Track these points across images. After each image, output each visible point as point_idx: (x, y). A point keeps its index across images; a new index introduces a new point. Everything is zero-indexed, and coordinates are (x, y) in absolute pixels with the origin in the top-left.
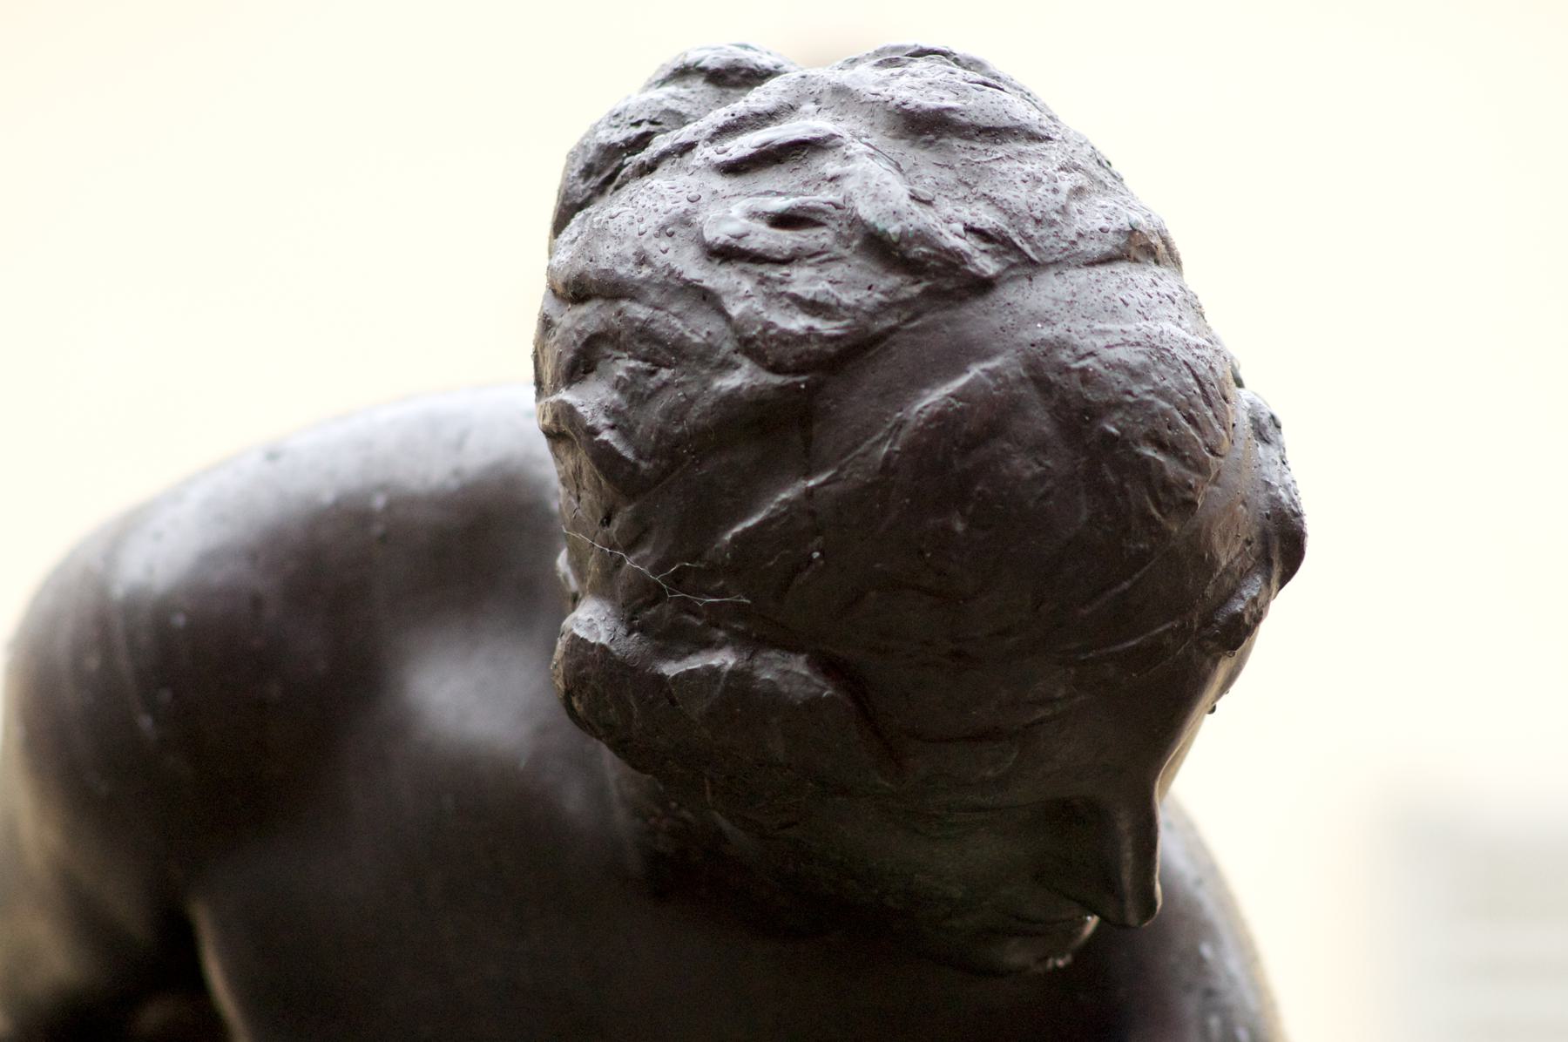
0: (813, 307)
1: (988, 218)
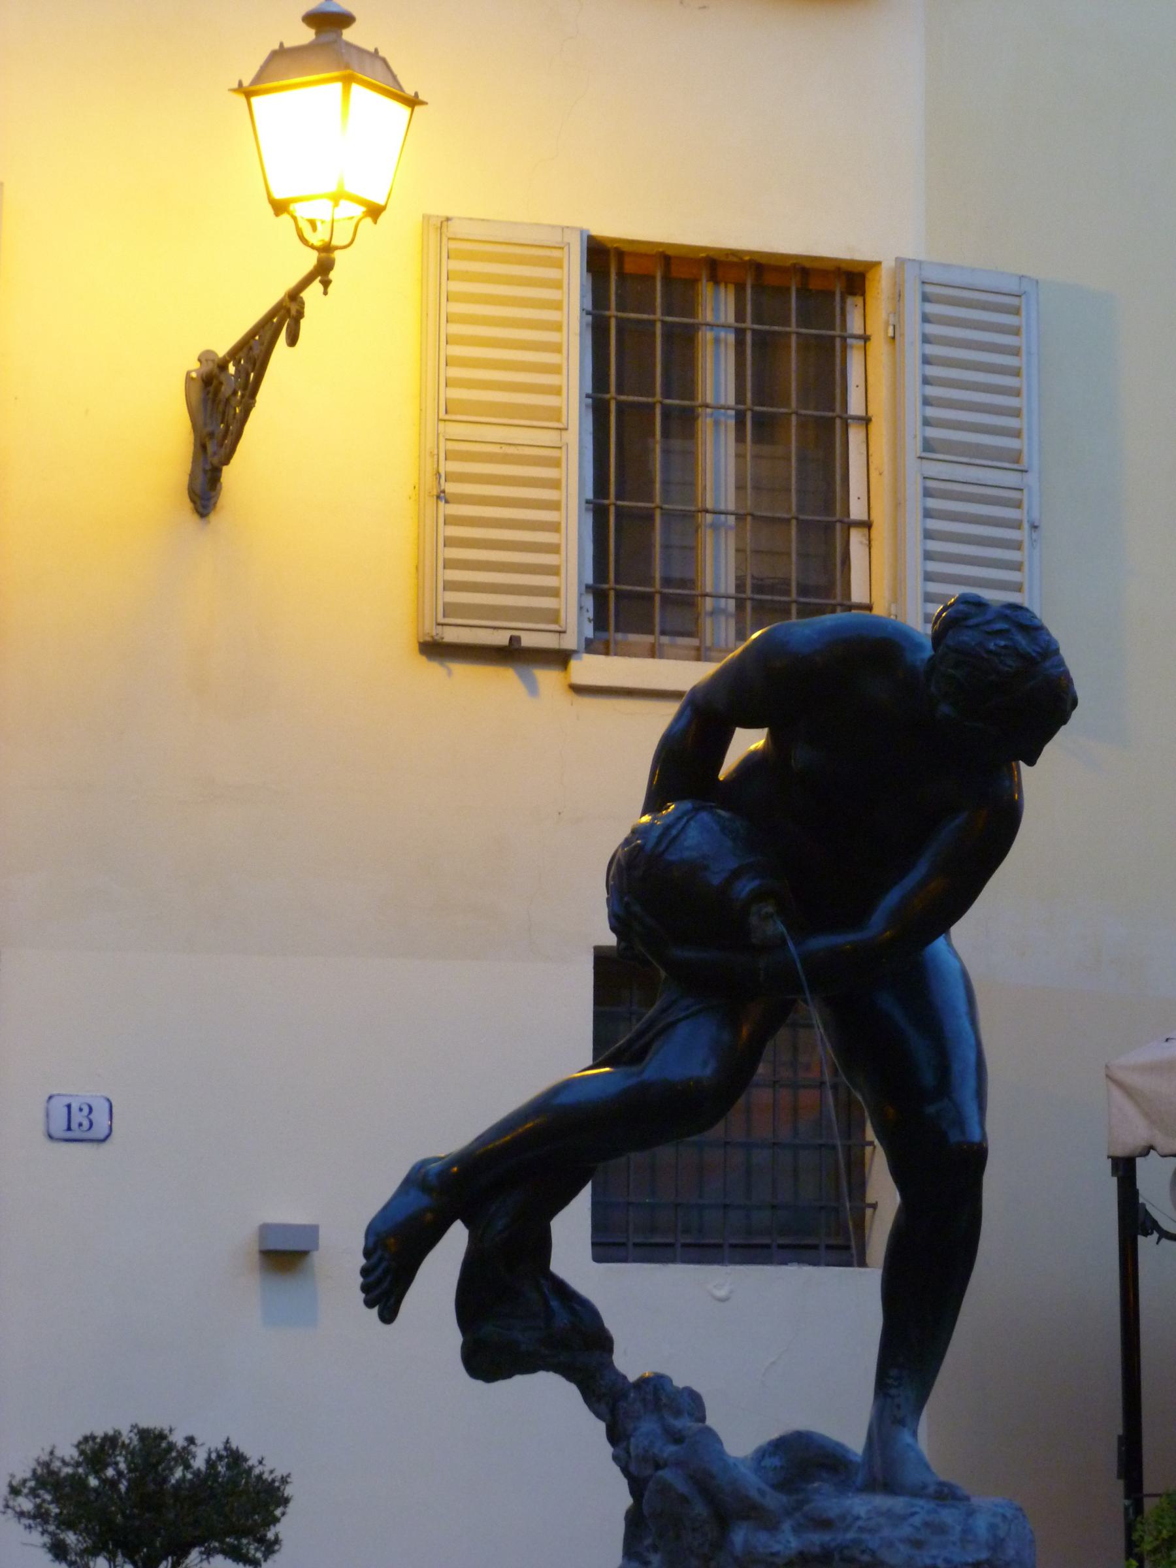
0: (1010, 666)
1: (1039, 650)
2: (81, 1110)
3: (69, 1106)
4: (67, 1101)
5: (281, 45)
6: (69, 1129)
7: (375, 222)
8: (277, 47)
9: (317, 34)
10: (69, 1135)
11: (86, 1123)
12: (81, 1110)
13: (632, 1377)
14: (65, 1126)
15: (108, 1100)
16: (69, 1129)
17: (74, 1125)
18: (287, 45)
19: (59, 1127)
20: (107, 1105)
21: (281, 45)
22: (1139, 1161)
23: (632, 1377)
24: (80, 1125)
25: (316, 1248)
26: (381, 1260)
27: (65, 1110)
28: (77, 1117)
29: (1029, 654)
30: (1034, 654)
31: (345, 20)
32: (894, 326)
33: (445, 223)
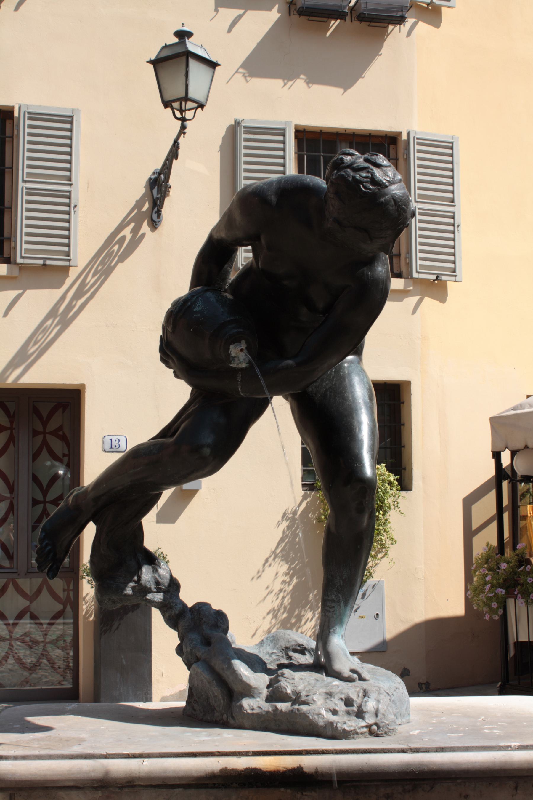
1: (388, 179)
2: (116, 441)
3: (111, 440)
4: (111, 437)
5: (166, 44)
6: (111, 448)
7: (202, 110)
8: (164, 45)
9: (179, 40)
10: (111, 450)
11: (118, 446)
12: (116, 441)
13: (190, 604)
14: (110, 447)
15: (126, 437)
16: (111, 448)
17: (113, 446)
18: (167, 44)
19: (108, 447)
20: (125, 439)
21: (166, 44)
22: (502, 453)
23: (190, 604)
24: (115, 446)
25: (201, 489)
26: (47, 545)
27: (110, 441)
28: (114, 443)
29: (381, 181)
30: (384, 181)
31: (189, 34)
32: (407, 155)
33: (242, 121)
